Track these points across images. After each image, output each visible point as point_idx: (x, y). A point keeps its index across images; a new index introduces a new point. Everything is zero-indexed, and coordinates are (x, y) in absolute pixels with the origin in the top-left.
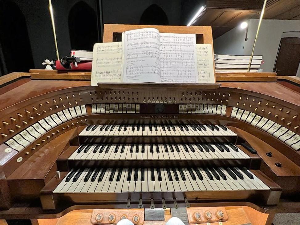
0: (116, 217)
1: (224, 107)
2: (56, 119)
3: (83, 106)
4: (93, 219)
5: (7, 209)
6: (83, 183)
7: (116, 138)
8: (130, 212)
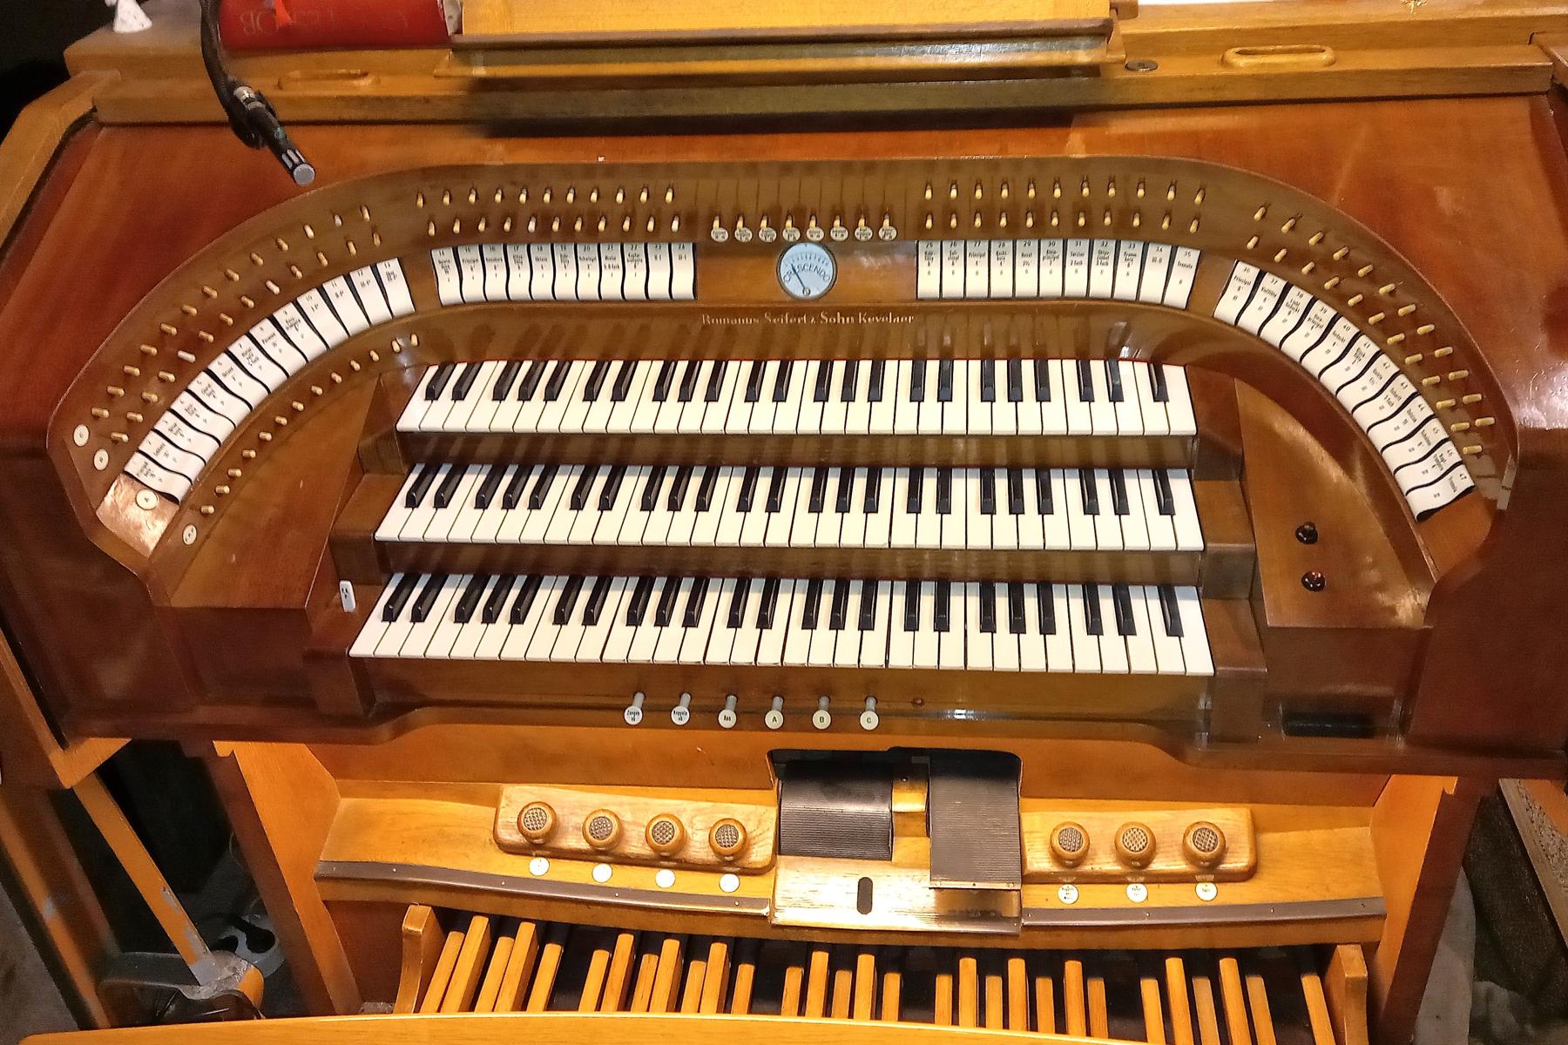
0: (626, 826)
1: (1186, 261)
3: (391, 267)
4: (507, 825)
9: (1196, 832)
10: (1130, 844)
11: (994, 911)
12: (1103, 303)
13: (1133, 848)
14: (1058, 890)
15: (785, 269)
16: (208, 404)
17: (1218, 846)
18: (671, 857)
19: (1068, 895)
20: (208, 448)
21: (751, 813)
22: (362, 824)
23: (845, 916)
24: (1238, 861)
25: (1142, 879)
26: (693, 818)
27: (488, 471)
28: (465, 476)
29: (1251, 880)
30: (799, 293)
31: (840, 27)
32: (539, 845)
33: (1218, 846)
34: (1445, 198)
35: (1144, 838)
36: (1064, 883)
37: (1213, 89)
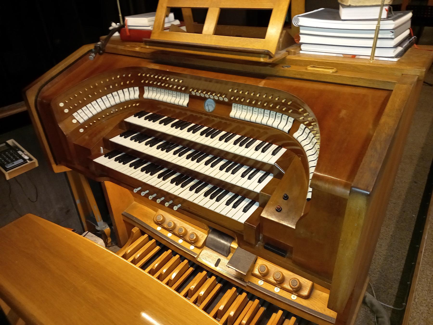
6: (202, 196)
8: (192, 229)
12: (270, 127)
15: (206, 104)
19: (261, 283)
20: (90, 115)
23: (212, 265)
25: (280, 287)
27: (248, 168)
28: (258, 173)
30: (207, 110)
31: (207, 45)
36: (262, 280)
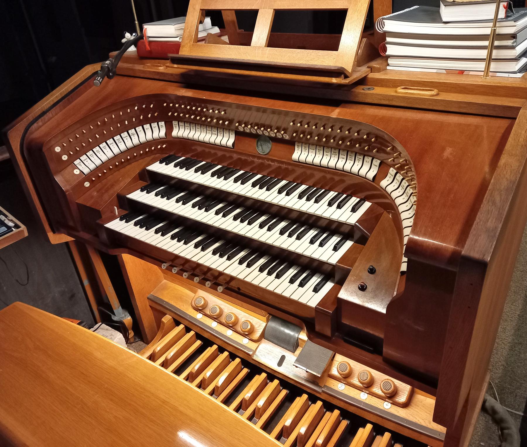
2: (127, 139)
5: (78, 231)
6: (257, 272)
7: (295, 211)
9: (385, 382)
10: (362, 377)
11: (317, 382)
13: (362, 378)
14: (339, 384)
16: (104, 152)
17: (391, 390)
18: (232, 326)
20: (98, 163)
21: (258, 322)
22: (165, 288)
24: (402, 398)
25: (368, 392)
26: (242, 318)
29: (405, 409)
32: (200, 310)
33: (391, 390)
34: (448, 152)
35: (367, 377)
37: (388, 100)
